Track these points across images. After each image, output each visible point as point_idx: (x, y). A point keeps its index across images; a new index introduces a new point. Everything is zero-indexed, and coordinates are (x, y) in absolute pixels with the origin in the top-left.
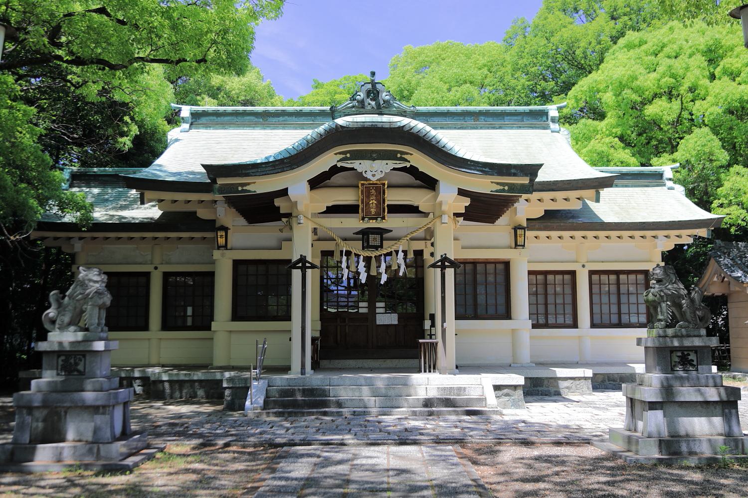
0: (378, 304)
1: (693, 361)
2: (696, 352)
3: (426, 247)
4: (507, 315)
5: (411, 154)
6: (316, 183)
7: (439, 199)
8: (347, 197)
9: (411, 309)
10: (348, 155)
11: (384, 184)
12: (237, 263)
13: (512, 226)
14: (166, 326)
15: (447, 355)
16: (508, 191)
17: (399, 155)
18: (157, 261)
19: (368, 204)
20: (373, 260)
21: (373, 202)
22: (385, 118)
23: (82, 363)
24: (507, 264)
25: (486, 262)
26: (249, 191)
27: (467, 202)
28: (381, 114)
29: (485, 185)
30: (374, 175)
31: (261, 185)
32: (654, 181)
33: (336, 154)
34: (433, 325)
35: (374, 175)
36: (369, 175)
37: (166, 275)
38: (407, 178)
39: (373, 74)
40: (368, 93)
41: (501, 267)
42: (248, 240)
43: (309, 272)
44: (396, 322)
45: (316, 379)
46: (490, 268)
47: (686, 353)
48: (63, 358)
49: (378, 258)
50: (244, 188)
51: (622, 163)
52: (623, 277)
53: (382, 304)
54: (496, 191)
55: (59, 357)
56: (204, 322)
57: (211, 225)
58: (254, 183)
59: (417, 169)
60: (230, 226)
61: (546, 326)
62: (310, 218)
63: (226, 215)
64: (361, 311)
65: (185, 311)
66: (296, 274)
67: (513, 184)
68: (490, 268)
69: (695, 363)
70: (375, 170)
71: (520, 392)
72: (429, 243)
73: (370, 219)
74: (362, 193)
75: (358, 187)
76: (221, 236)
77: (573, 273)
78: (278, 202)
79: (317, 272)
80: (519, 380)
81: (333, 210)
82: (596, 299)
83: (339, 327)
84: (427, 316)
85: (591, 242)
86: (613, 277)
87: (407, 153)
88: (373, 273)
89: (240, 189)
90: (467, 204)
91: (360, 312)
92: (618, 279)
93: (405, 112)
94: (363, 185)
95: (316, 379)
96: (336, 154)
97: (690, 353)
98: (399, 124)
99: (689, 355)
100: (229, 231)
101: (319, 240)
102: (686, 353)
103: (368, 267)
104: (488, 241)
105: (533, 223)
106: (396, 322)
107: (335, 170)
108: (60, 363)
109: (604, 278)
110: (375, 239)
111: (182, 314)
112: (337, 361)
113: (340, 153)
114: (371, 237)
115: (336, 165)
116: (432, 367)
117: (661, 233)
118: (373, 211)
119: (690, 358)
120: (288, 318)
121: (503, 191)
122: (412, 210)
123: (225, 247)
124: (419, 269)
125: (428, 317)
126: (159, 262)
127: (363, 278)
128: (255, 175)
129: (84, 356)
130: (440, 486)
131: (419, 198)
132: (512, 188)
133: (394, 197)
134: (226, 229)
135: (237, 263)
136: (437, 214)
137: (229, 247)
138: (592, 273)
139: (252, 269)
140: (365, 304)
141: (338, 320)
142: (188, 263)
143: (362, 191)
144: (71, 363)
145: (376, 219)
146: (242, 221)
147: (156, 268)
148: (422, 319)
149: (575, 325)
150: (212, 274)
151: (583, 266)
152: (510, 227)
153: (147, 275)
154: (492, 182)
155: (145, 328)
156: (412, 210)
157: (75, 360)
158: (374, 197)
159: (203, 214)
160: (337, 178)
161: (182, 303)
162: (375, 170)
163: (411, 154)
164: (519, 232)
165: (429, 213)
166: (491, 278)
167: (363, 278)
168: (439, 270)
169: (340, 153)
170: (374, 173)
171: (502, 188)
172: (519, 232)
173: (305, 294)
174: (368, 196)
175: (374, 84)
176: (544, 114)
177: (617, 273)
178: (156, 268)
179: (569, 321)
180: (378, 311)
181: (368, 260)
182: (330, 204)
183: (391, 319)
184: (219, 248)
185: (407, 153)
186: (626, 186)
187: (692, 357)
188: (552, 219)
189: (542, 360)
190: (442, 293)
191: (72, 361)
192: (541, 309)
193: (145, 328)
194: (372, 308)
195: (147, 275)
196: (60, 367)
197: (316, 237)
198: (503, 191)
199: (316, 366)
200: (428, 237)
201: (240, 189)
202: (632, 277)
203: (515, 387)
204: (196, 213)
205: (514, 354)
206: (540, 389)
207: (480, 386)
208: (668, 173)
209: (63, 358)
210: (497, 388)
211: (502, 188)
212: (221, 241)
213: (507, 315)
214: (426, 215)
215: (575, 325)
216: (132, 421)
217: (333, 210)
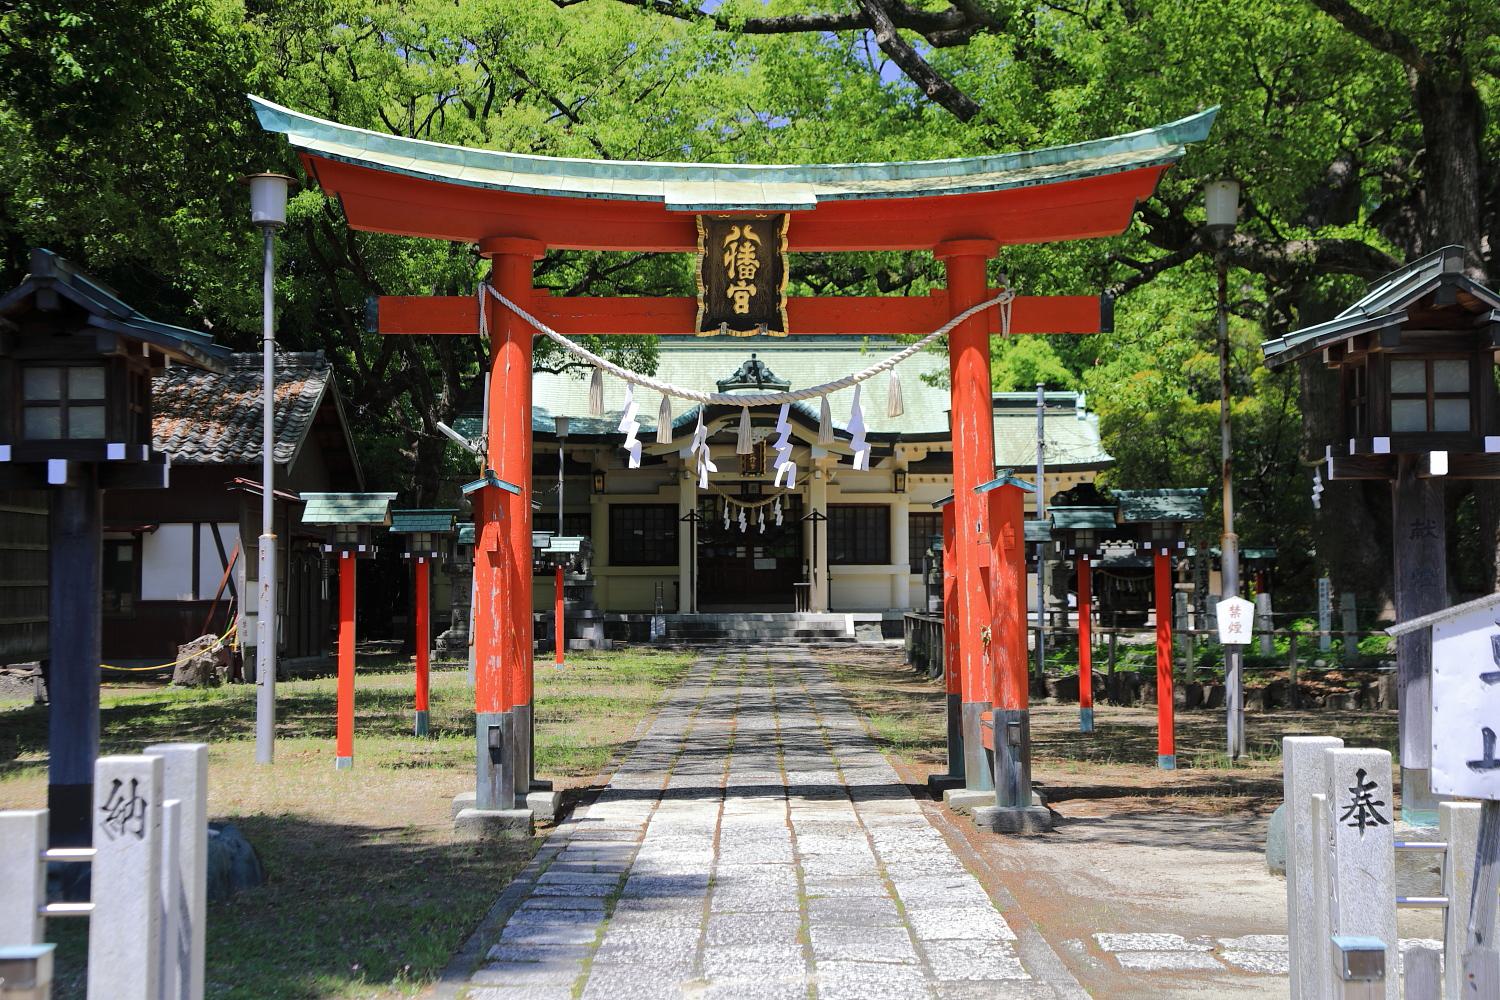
0: (756, 549)
4: (886, 560)
9: (790, 552)
12: (613, 507)
15: (819, 593)
24: (886, 509)
25: (866, 506)
28: (761, 388)
32: (1065, 411)
40: (750, 370)
41: (881, 511)
46: (871, 512)
49: (757, 510)
51: (450, 765)
53: (760, 549)
64: (739, 555)
68: (871, 512)
71: (878, 628)
80: (878, 617)
88: (753, 523)
91: (682, 523)
103: (748, 518)
105: (915, 467)
116: (806, 605)
117: (1064, 476)
123: (602, 492)
127: (743, 527)
134: (602, 473)
135: (613, 507)
164: (899, 476)
166: (871, 523)
167: (743, 527)
175: (755, 363)
181: (748, 511)
183: (770, 564)
184: (596, 492)
194: (750, 552)
203: (874, 623)
205: (893, 600)
207: (846, 622)
210: (857, 623)
213: (886, 560)
216: (1406, 319)
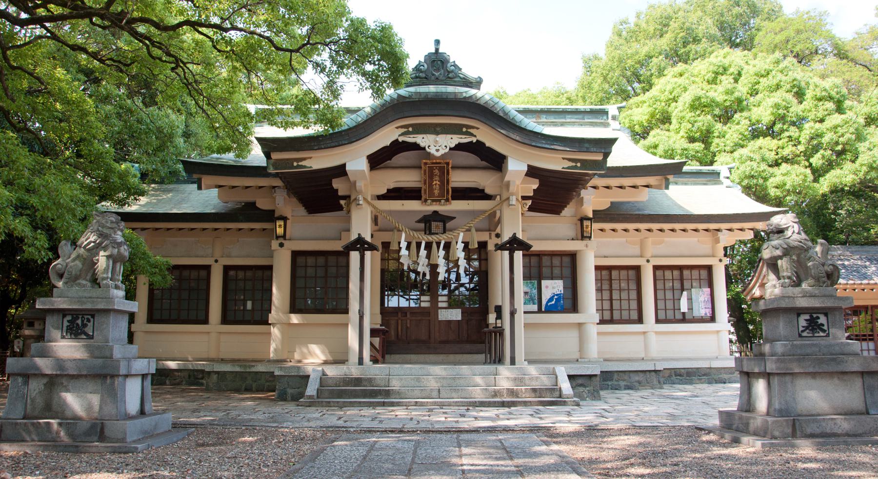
1: (823, 325)
2: (826, 315)
3: (490, 238)
5: (478, 128)
6: (377, 160)
7: (507, 179)
8: (409, 179)
10: (410, 129)
11: (448, 164)
12: (295, 254)
13: (579, 217)
14: (226, 319)
16: (580, 168)
17: (464, 130)
18: (217, 255)
19: (431, 185)
20: (434, 246)
21: (436, 182)
22: (450, 89)
23: (90, 325)
25: (552, 254)
26: (305, 167)
27: (534, 185)
29: (555, 162)
30: (437, 150)
31: (319, 161)
33: (397, 128)
34: (499, 316)
35: (437, 150)
36: (432, 150)
37: (227, 269)
38: (470, 158)
39: (437, 42)
42: (306, 231)
43: (368, 254)
44: (459, 318)
45: (378, 371)
47: (815, 316)
48: (69, 318)
50: (300, 164)
52: (686, 273)
54: (568, 168)
55: (64, 316)
56: (261, 318)
57: (270, 216)
58: (310, 158)
59: (484, 144)
60: (289, 216)
61: (611, 321)
62: (369, 199)
63: (284, 204)
64: (423, 305)
65: (245, 305)
66: (355, 256)
67: (586, 161)
69: (825, 328)
70: (438, 145)
72: (493, 234)
73: (433, 201)
74: (425, 174)
75: (421, 168)
76: (280, 226)
77: (637, 269)
78: (337, 184)
79: (378, 254)
81: (395, 194)
82: (660, 295)
83: (400, 322)
84: (492, 308)
85: (651, 239)
86: (676, 273)
87: (473, 127)
89: (295, 164)
90: (535, 187)
92: (682, 275)
93: (471, 83)
94: (426, 164)
95: (378, 371)
96: (397, 128)
97: (819, 315)
98: (464, 95)
99: (818, 318)
100: (288, 221)
101: (379, 230)
102: (815, 316)
104: (551, 233)
105: (600, 216)
106: (459, 318)
107: (397, 147)
108: (66, 324)
109: (668, 274)
110: (437, 226)
111: (242, 308)
112: (398, 356)
113: (402, 127)
114: (434, 224)
115: (397, 140)
118: (436, 192)
119: (820, 321)
120: (346, 311)
121: (575, 167)
122: (477, 194)
124: (483, 262)
125: (493, 309)
126: (219, 255)
128: (311, 149)
129: (93, 316)
130: (563, 457)
131: (483, 179)
132: (585, 164)
133: (459, 179)
134: (285, 219)
135: (295, 254)
136: (504, 197)
137: (287, 237)
138: (656, 268)
139: (311, 260)
140: (427, 298)
141: (400, 314)
142: (248, 256)
143: (425, 171)
144: (78, 324)
145: (440, 201)
146: (302, 211)
147: (216, 261)
148: (486, 313)
149: (640, 320)
150: (270, 268)
151: (648, 261)
152: (575, 219)
153: (208, 268)
154: (564, 159)
155: (206, 321)
156: (477, 194)
157: (83, 321)
158: (437, 178)
159: (263, 204)
160: (400, 158)
161: (242, 297)
162: (438, 145)
163: (478, 128)
164: (586, 223)
165: (496, 196)
168: (506, 253)
169: (402, 127)
170: (437, 148)
171: (574, 164)
172: (586, 223)
173: (363, 279)
174: (431, 176)
176: (605, 113)
177: (681, 268)
178: (216, 261)
179: (634, 315)
180: (440, 305)
181: (429, 246)
182: (392, 186)
184: (278, 237)
185: (473, 127)
186: (686, 184)
187: (822, 320)
188: (612, 214)
189: (607, 356)
190: (508, 278)
191: (79, 322)
192: (606, 305)
193: (206, 321)
195: (208, 268)
196: (65, 328)
197: (377, 228)
198: (575, 167)
199: (375, 360)
200: (492, 228)
201: (295, 164)
202: (695, 273)
204: (255, 203)
206: (610, 383)
208: (724, 172)
209: (69, 318)
211: (574, 164)
212: (280, 231)
214: (488, 197)
215: (640, 320)
217: (395, 194)
